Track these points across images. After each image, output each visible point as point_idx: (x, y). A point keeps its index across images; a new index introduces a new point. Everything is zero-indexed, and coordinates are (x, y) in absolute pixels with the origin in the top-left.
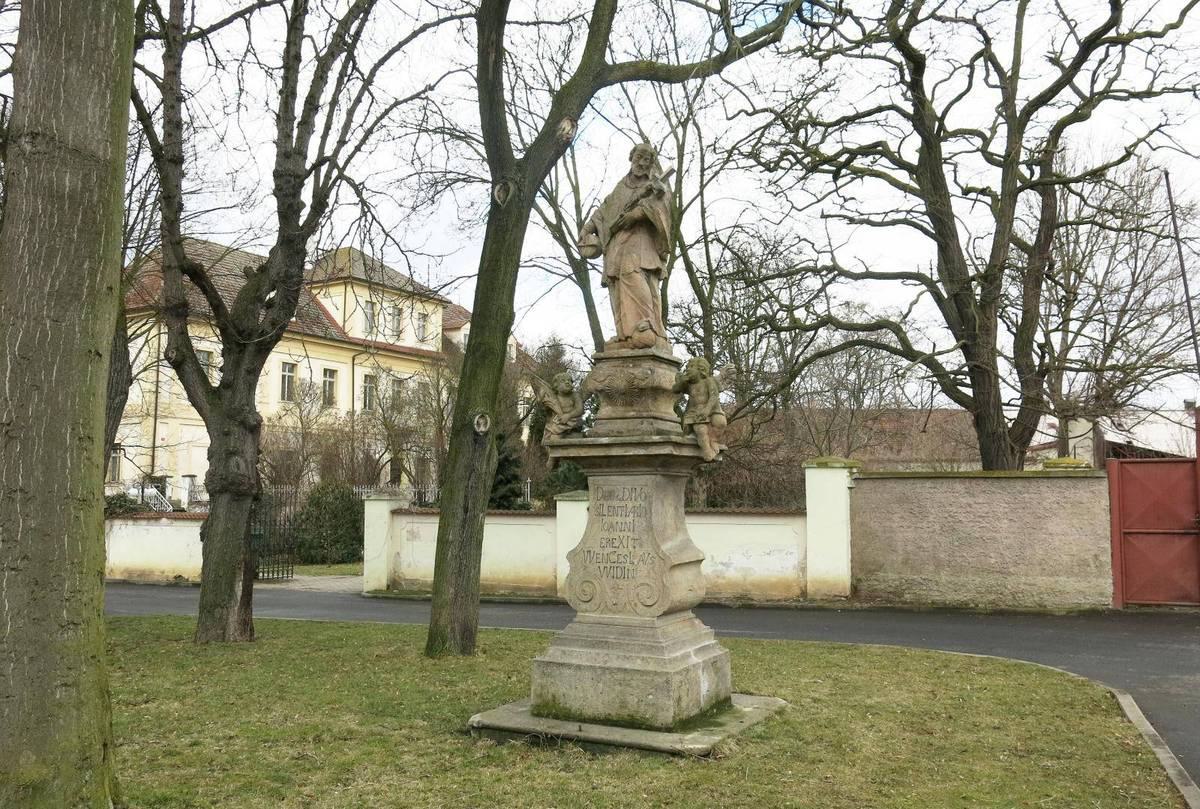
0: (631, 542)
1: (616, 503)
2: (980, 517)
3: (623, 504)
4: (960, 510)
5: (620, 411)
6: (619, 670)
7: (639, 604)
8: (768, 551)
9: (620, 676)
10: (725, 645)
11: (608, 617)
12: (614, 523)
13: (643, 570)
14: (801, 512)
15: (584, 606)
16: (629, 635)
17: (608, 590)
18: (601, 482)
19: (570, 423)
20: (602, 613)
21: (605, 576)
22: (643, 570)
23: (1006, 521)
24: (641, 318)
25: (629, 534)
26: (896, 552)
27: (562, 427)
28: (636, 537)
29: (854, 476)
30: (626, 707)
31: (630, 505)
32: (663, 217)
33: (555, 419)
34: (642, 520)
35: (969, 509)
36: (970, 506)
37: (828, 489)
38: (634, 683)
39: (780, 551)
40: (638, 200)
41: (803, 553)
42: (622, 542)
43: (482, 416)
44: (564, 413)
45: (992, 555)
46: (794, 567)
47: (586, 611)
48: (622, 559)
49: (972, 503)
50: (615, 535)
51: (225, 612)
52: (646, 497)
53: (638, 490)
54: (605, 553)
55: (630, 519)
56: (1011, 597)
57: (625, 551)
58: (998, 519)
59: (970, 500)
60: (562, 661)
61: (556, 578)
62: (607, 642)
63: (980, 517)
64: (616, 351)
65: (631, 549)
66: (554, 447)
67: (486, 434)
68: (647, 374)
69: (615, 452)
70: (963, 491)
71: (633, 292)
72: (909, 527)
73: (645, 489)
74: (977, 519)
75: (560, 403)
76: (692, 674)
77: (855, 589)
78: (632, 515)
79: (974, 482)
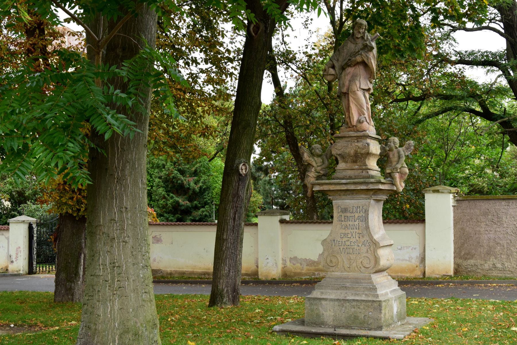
0: (357, 235)
1: (349, 214)
3: (353, 215)
5: (349, 165)
6: (354, 300)
7: (362, 267)
8: (400, 247)
9: (354, 303)
10: (402, 290)
11: (345, 274)
12: (348, 226)
13: (364, 249)
16: (358, 283)
18: (340, 204)
19: (321, 172)
21: (343, 253)
24: (361, 116)
25: (356, 231)
26: (483, 246)
27: (316, 174)
28: (360, 232)
29: (456, 198)
30: (358, 319)
31: (357, 215)
32: (373, 61)
33: (313, 170)
37: (440, 206)
38: (362, 307)
39: (408, 247)
40: (359, 51)
41: (422, 251)
43: (244, 165)
44: (318, 166)
48: (352, 244)
50: (349, 231)
51: (73, 285)
53: (361, 208)
54: (343, 241)
55: (357, 223)
57: (354, 240)
60: (322, 297)
61: (257, 267)
62: (345, 287)
64: (347, 133)
65: (357, 238)
66: (313, 185)
67: (246, 175)
68: (365, 146)
69: (352, 187)
71: (355, 101)
72: (491, 231)
75: (315, 161)
76: (390, 303)
77: (457, 271)
78: (358, 221)
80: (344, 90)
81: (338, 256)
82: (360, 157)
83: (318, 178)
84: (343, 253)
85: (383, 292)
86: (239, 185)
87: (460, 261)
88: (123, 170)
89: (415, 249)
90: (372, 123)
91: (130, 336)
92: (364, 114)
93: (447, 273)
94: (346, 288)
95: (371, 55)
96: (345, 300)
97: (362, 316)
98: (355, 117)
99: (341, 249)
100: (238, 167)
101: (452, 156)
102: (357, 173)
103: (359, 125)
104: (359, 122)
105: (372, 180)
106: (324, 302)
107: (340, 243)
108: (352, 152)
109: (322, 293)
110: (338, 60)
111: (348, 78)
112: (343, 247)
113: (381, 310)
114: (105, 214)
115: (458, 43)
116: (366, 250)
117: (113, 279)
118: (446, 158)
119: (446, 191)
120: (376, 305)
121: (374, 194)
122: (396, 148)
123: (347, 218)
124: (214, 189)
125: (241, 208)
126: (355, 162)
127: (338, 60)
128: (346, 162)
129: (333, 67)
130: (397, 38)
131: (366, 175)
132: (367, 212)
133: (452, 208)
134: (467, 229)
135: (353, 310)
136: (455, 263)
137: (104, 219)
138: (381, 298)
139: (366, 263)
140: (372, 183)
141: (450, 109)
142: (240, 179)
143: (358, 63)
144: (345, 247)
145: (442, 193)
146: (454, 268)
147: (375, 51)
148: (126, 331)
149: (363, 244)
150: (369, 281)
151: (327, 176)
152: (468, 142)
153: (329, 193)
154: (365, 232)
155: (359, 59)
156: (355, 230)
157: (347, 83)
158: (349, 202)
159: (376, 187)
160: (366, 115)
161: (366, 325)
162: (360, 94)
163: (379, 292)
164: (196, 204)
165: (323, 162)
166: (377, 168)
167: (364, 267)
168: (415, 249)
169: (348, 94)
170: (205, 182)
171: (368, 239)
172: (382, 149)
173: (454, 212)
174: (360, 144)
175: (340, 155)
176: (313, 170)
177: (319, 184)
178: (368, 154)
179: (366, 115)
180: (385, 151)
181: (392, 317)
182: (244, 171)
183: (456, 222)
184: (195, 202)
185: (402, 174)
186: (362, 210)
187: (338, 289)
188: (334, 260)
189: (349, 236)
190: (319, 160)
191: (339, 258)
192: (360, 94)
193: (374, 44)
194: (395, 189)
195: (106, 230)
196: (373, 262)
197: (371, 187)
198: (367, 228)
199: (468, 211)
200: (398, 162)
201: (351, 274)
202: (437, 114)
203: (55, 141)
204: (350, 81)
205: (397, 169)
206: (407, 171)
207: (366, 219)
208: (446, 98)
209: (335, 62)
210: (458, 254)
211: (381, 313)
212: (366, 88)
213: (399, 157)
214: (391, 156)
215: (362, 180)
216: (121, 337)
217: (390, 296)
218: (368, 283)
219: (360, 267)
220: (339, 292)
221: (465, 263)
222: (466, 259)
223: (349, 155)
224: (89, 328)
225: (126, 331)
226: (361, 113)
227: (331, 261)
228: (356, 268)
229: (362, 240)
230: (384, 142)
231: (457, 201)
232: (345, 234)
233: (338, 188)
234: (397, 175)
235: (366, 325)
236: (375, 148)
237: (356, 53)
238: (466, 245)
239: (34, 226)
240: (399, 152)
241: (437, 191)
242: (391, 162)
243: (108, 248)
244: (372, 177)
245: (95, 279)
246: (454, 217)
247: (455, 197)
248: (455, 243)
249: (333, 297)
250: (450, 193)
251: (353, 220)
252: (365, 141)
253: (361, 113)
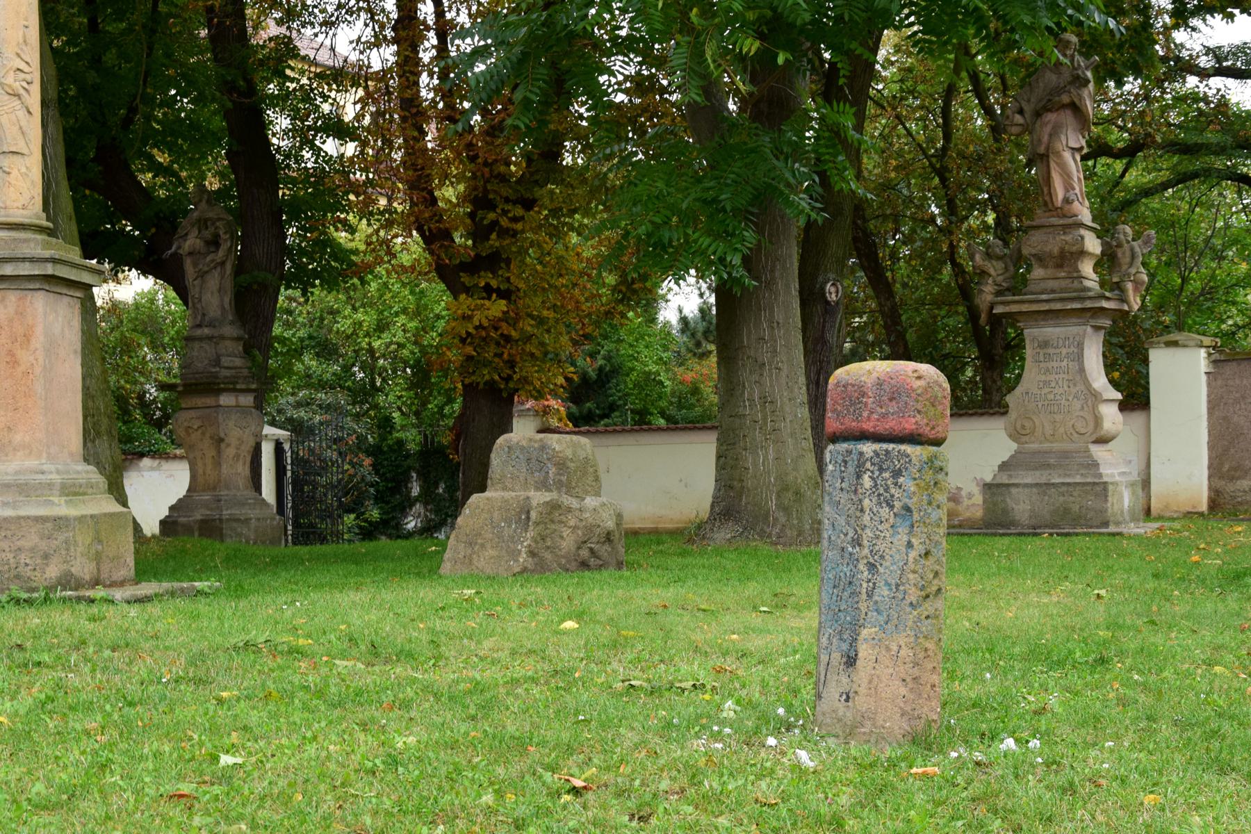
0: (1066, 384)
1: (1051, 351)
3: (1058, 351)
9: (1064, 489)
11: (1046, 446)
13: (1077, 405)
29: (1213, 357)
31: (1064, 351)
33: (990, 281)
38: (1075, 494)
41: (1143, 466)
50: (1051, 377)
55: (1065, 363)
67: (837, 303)
69: (1058, 306)
80: (1042, 150)
81: (1034, 417)
82: (1069, 258)
83: (999, 293)
85: (1109, 472)
86: (824, 321)
87: (1220, 484)
88: (772, 271)
90: (1087, 203)
91: (790, 495)
92: (1074, 189)
93: (1194, 507)
94: (1049, 466)
95: (1085, 93)
96: (1049, 485)
97: (1076, 508)
98: (1060, 194)
100: (823, 289)
101: (1195, 285)
102: (1064, 283)
103: (1067, 207)
104: (1067, 201)
105: (1091, 294)
106: (1014, 490)
108: (1056, 251)
109: (1010, 476)
110: (1029, 101)
111: (1048, 129)
113: (1106, 496)
114: (750, 332)
115: (1212, 27)
117: (765, 419)
118: (1182, 289)
119: (1192, 343)
120: (1098, 488)
121: (1092, 317)
122: (1128, 242)
123: (1048, 357)
124: (628, 375)
125: (829, 362)
126: (1059, 266)
127: (1029, 101)
128: (1045, 267)
129: (1021, 112)
130: (1111, 48)
131: (1080, 286)
132: (1080, 346)
133: (1204, 378)
134: (1236, 418)
135: (1061, 499)
136: (1210, 488)
137: (748, 338)
138: (1105, 479)
139: (1080, 426)
140: (1090, 298)
141: (1195, 175)
142: (826, 312)
143: (1064, 106)
145: (1185, 346)
146: (1210, 498)
147: (1091, 86)
148: (786, 488)
151: (1013, 290)
152: (1231, 253)
153: (1019, 318)
154: (1078, 378)
155: (1065, 99)
156: (1062, 376)
157: (1045, 139)
158: (1051, 331)
159: (1097, 305)
160: (1077, 191)
161: (1082, 522)
162: (1067, 155)
163: (1102, 470)
164: (590, 410)
165: (1006, 269)
166: (1094, 276)
169: (1048, 156)
170: (611, 357)
171: (1083, 388)
172: (1104, 244)
173: (1209, 385)
174: (1068, 238)
175: (1034, 255)
176: (990, 281)
177: (1003, 303)
178: (1082, 253)
179: (1077, 191)
180: (1111, 247)
181: (1122, 512)
182: (833, 296)
183: (1213, 406)
184: (588, 405)
185: (1137, 284)
187: (1036, 469)
188: (1028, 424)
189: (1053, 384)
190: (1000, 265)
192: (1067, 155)
193: (1089, 74)
194: (1126, 308)
195: (752, 353)
196: (1092, 425)
197: (1089, 304)
198: (1082, 370)
199: (1237, 382)
200: (1131, 265)
201: (1056, 446)
202: (1165, 186)
203: (730, 229)
204: (1050, 135)
205: (1129, 275)
206: (1146, 278)
207: (1080, 357)
208: (1187, 150)
209: (1024, 104)
210: (1215, 470)
211: (1106, 501)
212: (1077, 146)
213: (1133, 256)
214: (1120, 255)
215: (1075, 294)
216: (778, 497)
217: (1117, 478)
220: (1038, 473)
221: (1230, 487)
222: (1232, 479)
223: (1051, 255)
224: (731, 487)
225: (786, 488)
226: (1068, 187)
227: (1023, 427)
229: (1074, 390)
230: (1105, 231)
231: (1215, 362)
233: (1035, 307)
234: (1130, 286)
235: (1082, 522)
236: (1093, 245)
237: (1059, 90)
238: (1232, 451)
239: (287, 447)
240: (1132, 249)
241: (1175, 344)
242: (1120, 265)
243: (755, 377)
244: (1089, 289)
245: (738, 421)
246: (1208, 396)
247: (1209, 354)
248: (1211, 447)
249: (1029, 480)
250: (1202, 346)
252: (1076, 233)
253: (1068, 187)
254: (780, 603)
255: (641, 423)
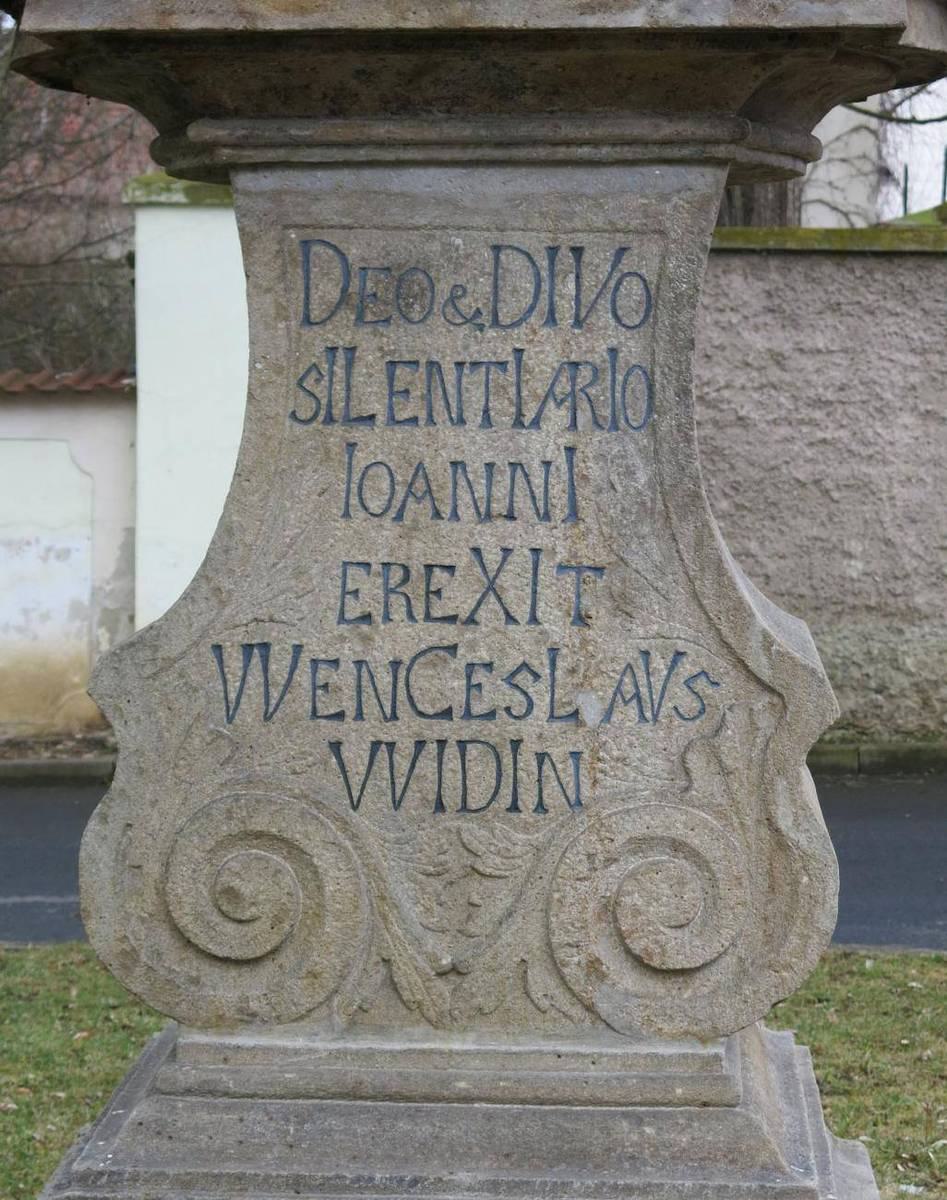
0: (555, 591)
1: (443, 342)
2: (819, 403)
3: (494, 345)
4: (740, 379)
11: (396, 1047)
13: (639, 754)
14: (128, 397)
15: (226, 989)
17: (401, 889)
18: (328, 210)
20: (352, 1026)
21: (376, 800)
22: (639, 754)
23: (907, 419)
25: (542, 536)
28: (592, 552)
31: (546, 353)
34: (632, 446)
35: (775, 374)
36: (778, 359)
42: (491, 587)
45: (855, 546)
46: (76, 610)
47: (248, 1018)
48: (495, 693)
49: (787, 348)
50: (452, 542)
52: (650, 303)
53: (599, 259)
55: (545, 443)
56: (913, 701)
57: (522, 644)
58: (882, 412)
59: (784, 341)
63: (819, 403)
65: (557, 626)
70: (757, 304)
73: (646, 258)
74: (805, 413)
78: (557, 416)
79: (799, 267)
81: (314, 839)
84: (376, 800)
89: (64, 555)
99: (356, 755)
107: (345, 678)
112: (374, 728)
116: (658, 764)
139: (658, 905)
144: (404, 731)
149: (634, 696)
150: (713, 1133)
156: (522, 535)
167: (640, 963)
168: (64, 555)
171: (683, 630)
186: (612, 290)
188: (263, 883)
189: (459, 597)
191: (325, 859)
218: (703, 1160)
219: (594, 967)
228: (541, 980)
232: (398, 577)
251: (502, 408)
254: (543, 126)
255: (131, 594)
